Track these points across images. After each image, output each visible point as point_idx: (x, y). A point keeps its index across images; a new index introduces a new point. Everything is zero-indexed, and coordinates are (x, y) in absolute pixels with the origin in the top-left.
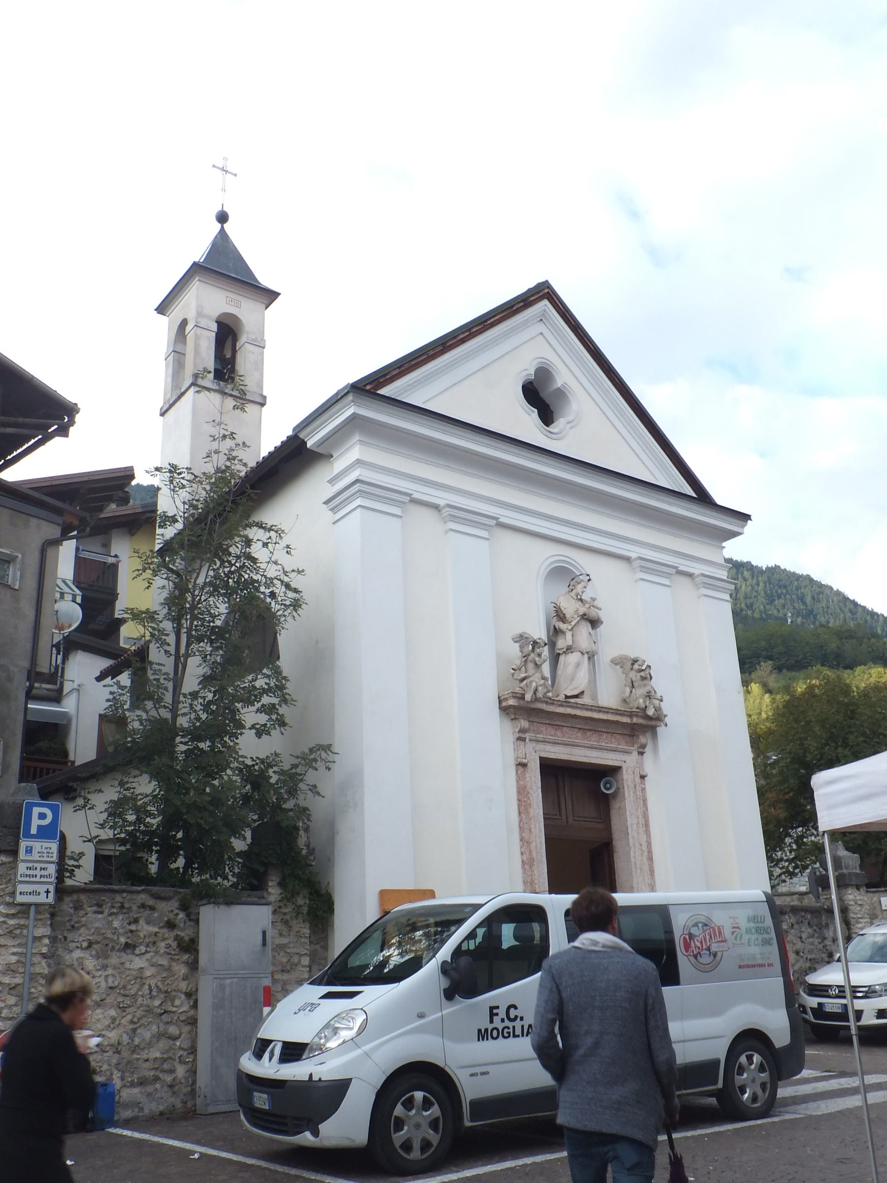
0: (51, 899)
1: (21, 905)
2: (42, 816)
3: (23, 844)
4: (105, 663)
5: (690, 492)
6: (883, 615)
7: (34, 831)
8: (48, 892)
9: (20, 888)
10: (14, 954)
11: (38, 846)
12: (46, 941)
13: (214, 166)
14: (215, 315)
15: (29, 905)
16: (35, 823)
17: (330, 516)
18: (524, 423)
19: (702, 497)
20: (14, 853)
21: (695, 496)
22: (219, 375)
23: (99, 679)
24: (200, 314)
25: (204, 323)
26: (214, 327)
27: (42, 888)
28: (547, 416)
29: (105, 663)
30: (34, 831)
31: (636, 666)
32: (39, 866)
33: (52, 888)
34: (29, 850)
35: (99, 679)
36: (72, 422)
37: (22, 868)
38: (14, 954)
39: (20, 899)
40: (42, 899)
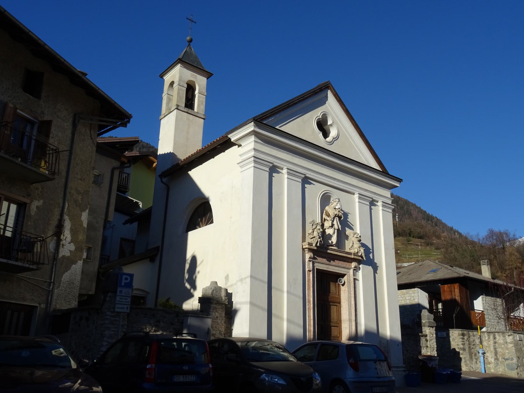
0: (128, 311)
1: (117, 312)
2: (126, 279)
3: (119, 289)
4: (127, 218)
5: (378, 168)
6: (436, 217)
7: (123, 284)
8: (127, 308)
9: (117, 306)
10: (113, 331)
11: (124, 290)
12: (126, 327)
13: (195, 23)
14: (186, 81)
15: (120, 312)
16: (124, 281)
17: (240, 169)
18: (318, 138)
19: (384, 172)
20: (115, 292)
21: (380, 169)
22: (186, 106)
23: (124, 224)
24: (180, 80)
25: (182, 84)
26: (186, 86)
27: (125, 306)
28: (326, 134)
29: (127, 218)
30: (123, 284)
31: (355, 236)
32: (124, 298)
33: (129, 307)
34: (121, 292)
35: (124, 224)
36: (129, 122)
37: (118, 298)
38: (113, 331)
39: (117, 310)
40: (125, 310)
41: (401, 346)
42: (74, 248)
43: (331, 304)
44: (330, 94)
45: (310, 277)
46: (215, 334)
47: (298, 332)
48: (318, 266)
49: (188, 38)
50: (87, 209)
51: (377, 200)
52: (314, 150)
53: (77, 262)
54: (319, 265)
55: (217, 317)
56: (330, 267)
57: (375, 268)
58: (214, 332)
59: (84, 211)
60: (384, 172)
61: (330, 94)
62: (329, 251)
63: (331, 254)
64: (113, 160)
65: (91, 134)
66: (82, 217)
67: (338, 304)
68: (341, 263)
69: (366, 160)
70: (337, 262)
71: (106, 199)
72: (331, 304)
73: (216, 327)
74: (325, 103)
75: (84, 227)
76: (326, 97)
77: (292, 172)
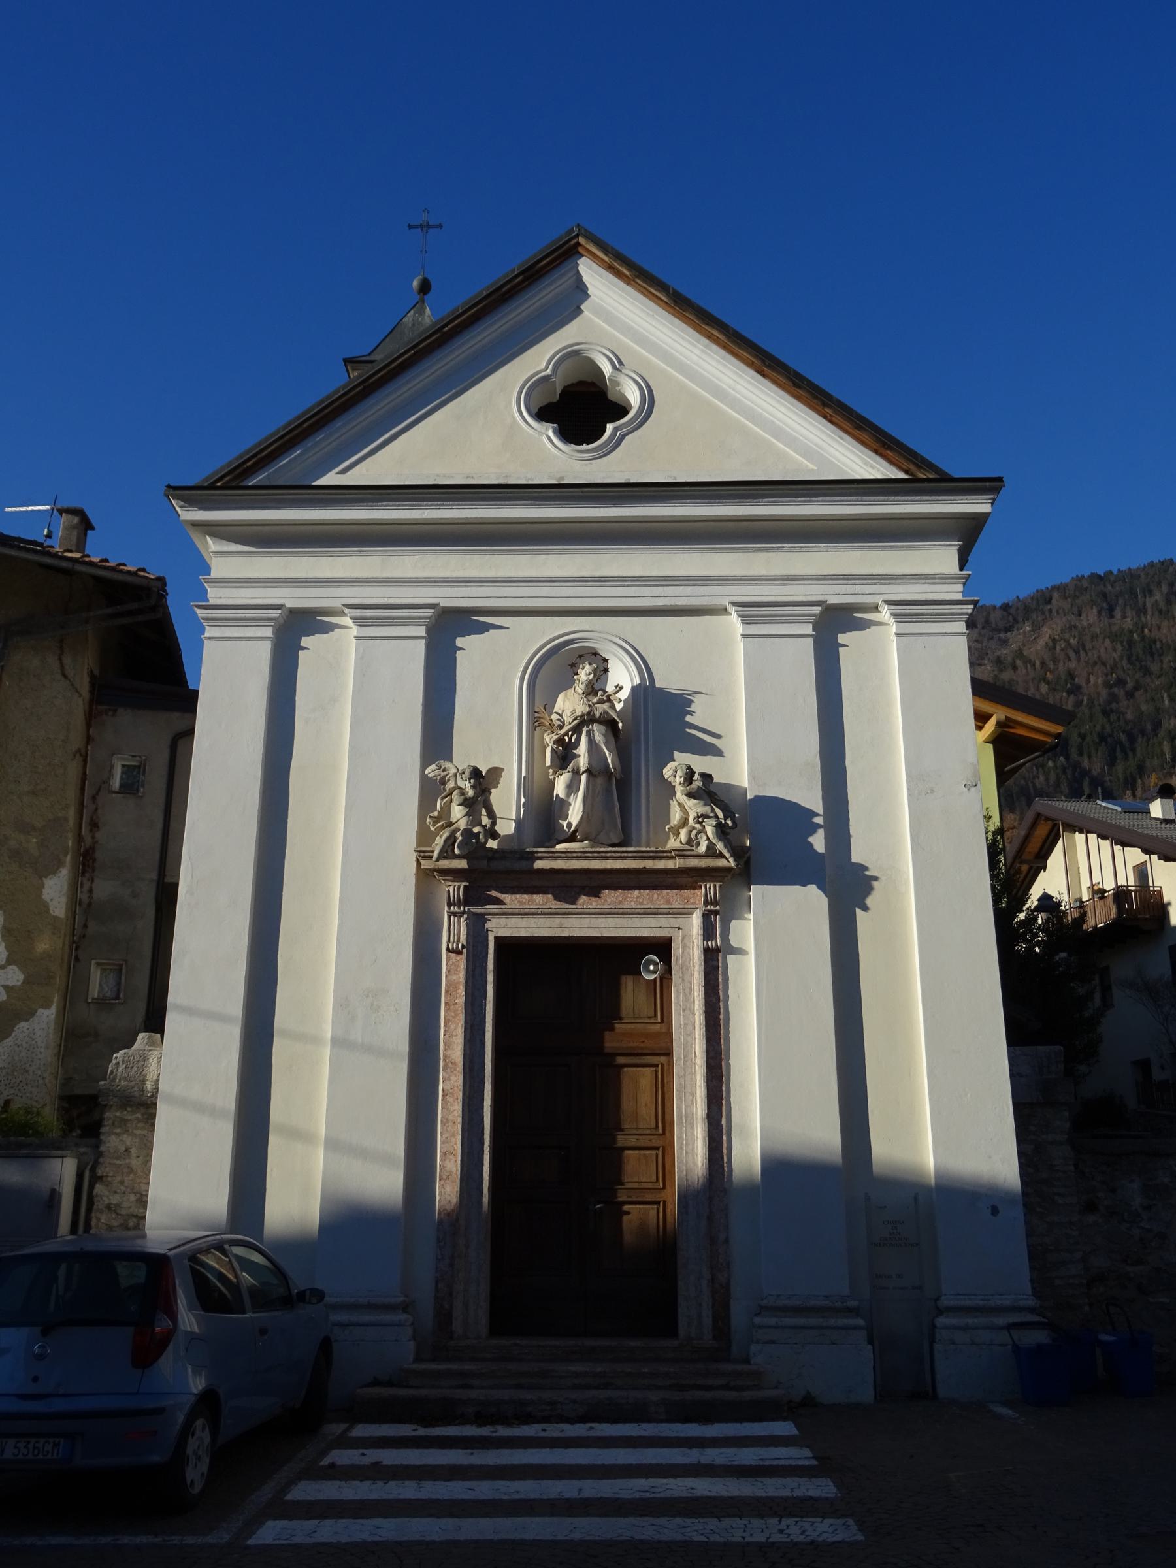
21: (901, 475)
41: (1019, 1212)
42: (21, 977)
43: (621, 1060)
44: (589, 271)
45: (452, 974)
46: (118, 1205)
47: (385, 1183)
48: (500, 927)
49: (415, 283)
50: (60, 864)
51: (868, 600)
52: (460, 507)
53: (32, 1013)
54: (502, 920)
55: (127, 1150)
56: (573, 921)
57: (848, 888)
58: (115, 1199)
59: (52, 871)
60: (925, 477)
61: (589, 271)
62: (539, 865)
63: (553, 871)
64: (176, 714)
65: (62, 667)
66: (45, 891)
67: (663, 1059)
68: (635, 899)
69: (808, 453)
70: (610, 898)
71: (159, 825)
72: (621, 1060)
73: (122, 1183)
74: (578, 311)
75: (55, 918)
76: (580, 290)
77: (369, 613)
